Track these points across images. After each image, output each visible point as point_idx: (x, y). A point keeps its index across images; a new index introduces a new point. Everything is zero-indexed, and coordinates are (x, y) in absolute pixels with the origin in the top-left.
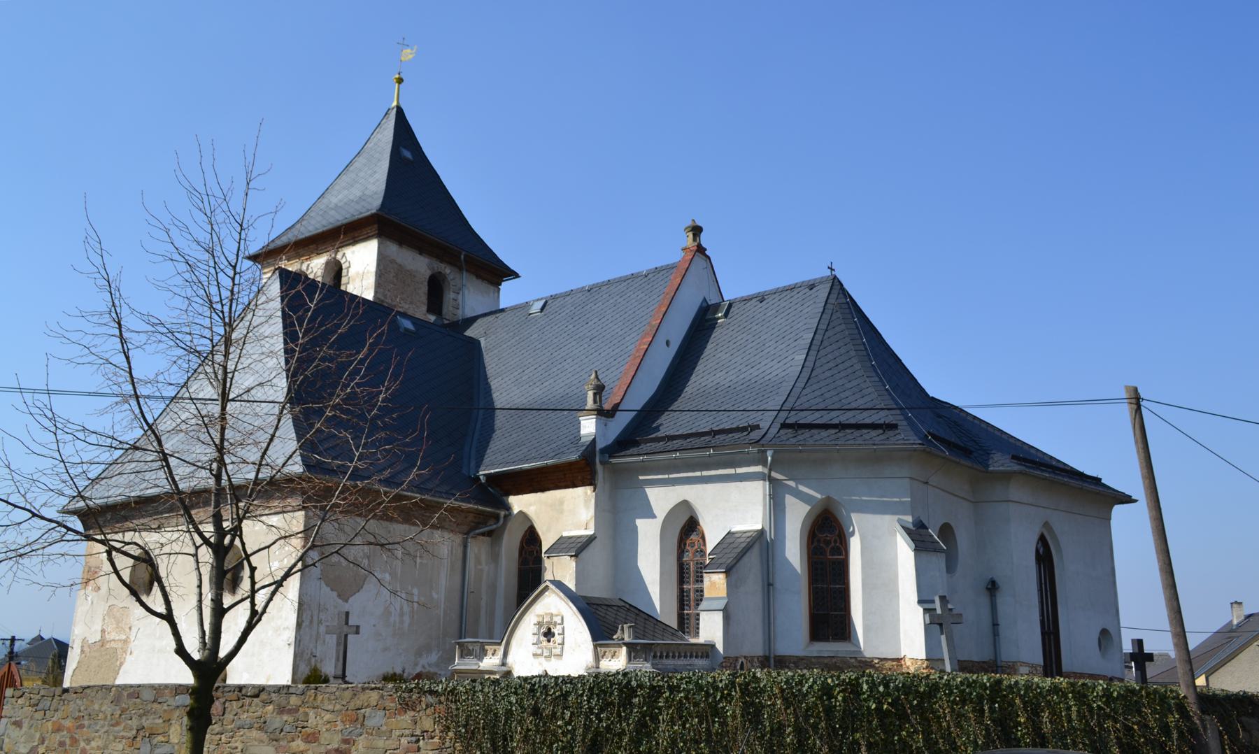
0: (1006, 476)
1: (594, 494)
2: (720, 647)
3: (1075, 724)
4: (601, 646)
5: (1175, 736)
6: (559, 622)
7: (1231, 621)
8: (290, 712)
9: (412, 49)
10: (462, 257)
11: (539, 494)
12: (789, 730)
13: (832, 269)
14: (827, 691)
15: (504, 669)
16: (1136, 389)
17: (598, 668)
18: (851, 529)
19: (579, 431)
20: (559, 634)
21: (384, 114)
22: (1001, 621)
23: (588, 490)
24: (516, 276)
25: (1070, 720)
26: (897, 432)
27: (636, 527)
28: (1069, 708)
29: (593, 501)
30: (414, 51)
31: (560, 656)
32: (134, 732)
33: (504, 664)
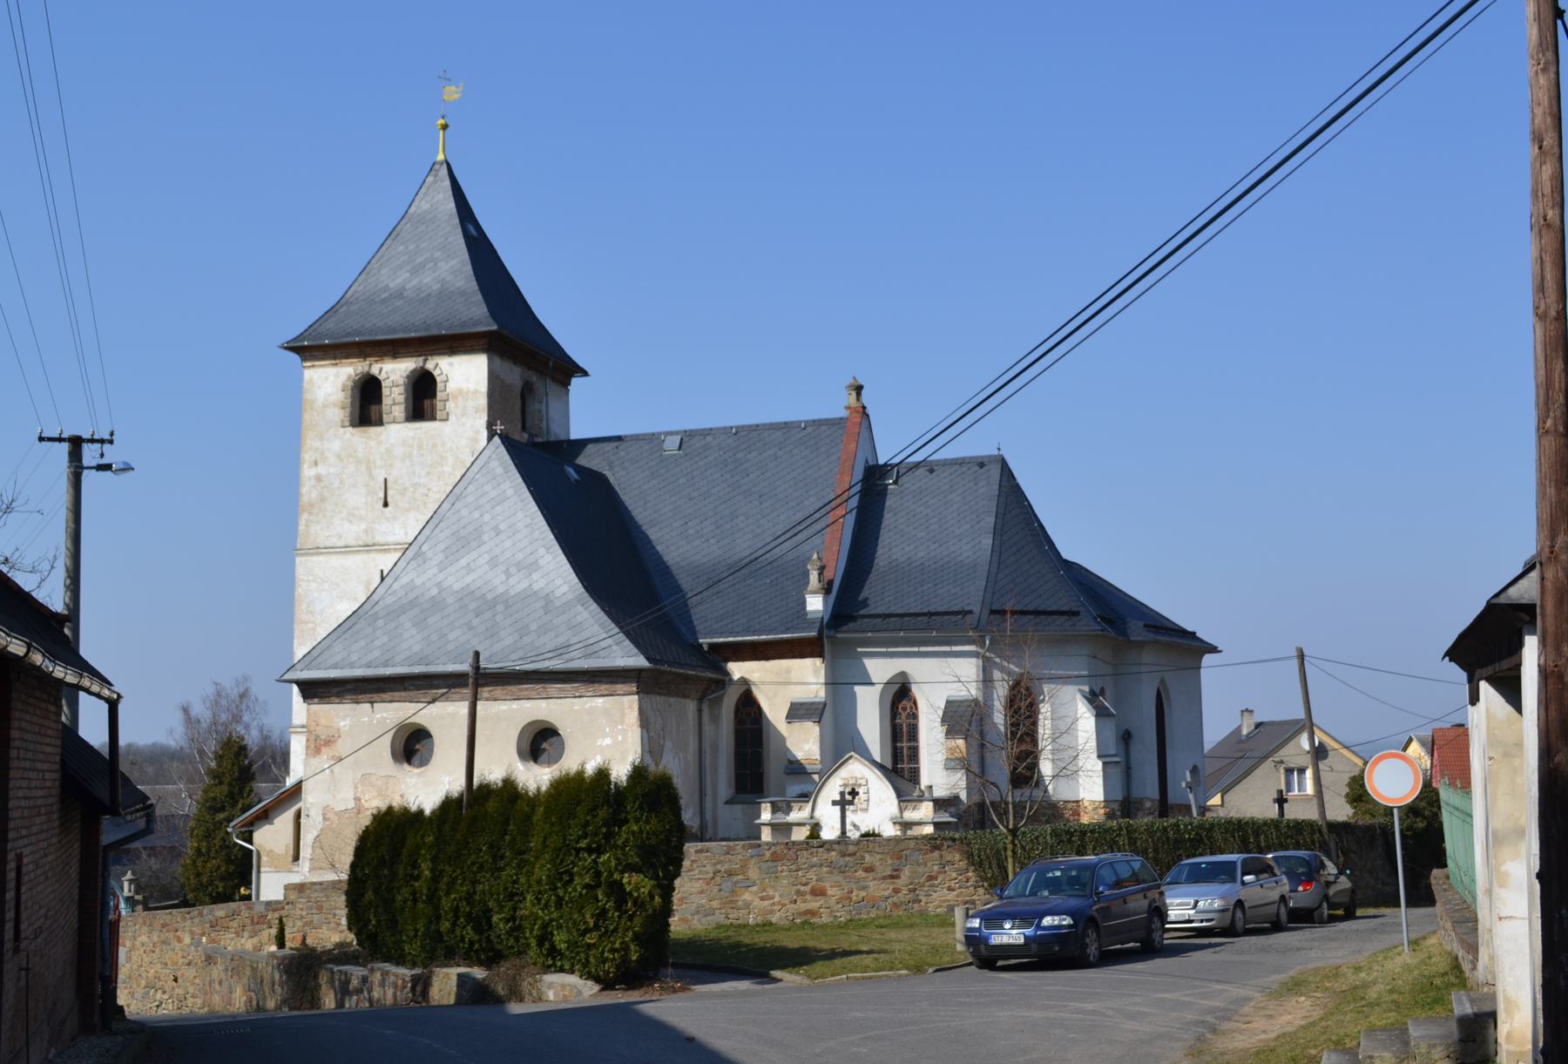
0: (1141, 645)
1: (823, 665)
2: (963, 796)
3: (1275, 841)
4: (903, 801)
5: (1317, 846)
6: (864, 783)
7: (1239, 728)
8: (849, 855)
9: (457, 87)
10: (551, 363)
11: (762, 662)
12: (1150, 850)
13: (999, 449)
14: (1165, 829)
15: (813, 821)
16: (1301, 650)
17: (902, 817)
18: (1042, 698)
19: (805, 607)
20: (864, 793)
21: (428, 170)
22: (1134, 765)
23: (818, 661)
24: (585, 373)
25: (1273, 840)
26: (1079, 617)
27: (855, 693)
28: (1272, 833)
29: (823, 672)
30: (461, 89)
31: (866, 810)
32: (712, 875)
33: (812, 817)
